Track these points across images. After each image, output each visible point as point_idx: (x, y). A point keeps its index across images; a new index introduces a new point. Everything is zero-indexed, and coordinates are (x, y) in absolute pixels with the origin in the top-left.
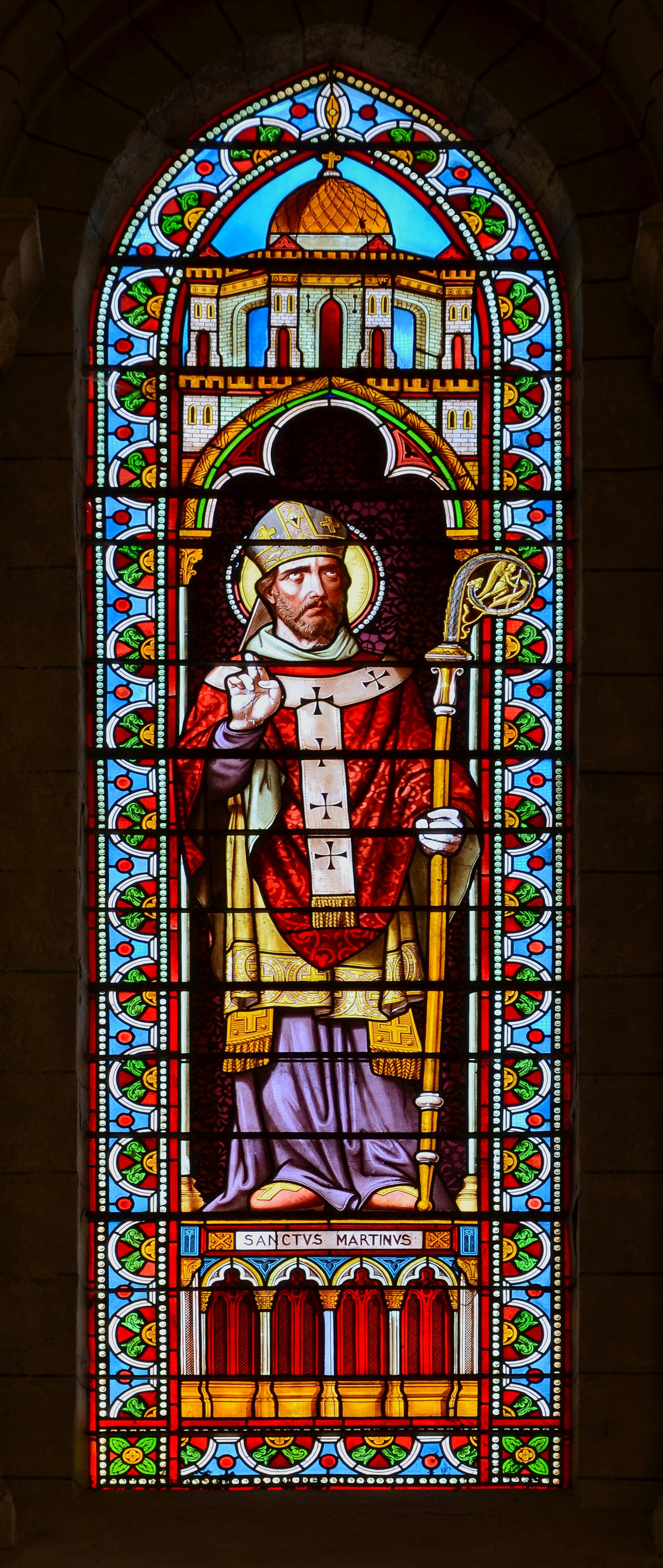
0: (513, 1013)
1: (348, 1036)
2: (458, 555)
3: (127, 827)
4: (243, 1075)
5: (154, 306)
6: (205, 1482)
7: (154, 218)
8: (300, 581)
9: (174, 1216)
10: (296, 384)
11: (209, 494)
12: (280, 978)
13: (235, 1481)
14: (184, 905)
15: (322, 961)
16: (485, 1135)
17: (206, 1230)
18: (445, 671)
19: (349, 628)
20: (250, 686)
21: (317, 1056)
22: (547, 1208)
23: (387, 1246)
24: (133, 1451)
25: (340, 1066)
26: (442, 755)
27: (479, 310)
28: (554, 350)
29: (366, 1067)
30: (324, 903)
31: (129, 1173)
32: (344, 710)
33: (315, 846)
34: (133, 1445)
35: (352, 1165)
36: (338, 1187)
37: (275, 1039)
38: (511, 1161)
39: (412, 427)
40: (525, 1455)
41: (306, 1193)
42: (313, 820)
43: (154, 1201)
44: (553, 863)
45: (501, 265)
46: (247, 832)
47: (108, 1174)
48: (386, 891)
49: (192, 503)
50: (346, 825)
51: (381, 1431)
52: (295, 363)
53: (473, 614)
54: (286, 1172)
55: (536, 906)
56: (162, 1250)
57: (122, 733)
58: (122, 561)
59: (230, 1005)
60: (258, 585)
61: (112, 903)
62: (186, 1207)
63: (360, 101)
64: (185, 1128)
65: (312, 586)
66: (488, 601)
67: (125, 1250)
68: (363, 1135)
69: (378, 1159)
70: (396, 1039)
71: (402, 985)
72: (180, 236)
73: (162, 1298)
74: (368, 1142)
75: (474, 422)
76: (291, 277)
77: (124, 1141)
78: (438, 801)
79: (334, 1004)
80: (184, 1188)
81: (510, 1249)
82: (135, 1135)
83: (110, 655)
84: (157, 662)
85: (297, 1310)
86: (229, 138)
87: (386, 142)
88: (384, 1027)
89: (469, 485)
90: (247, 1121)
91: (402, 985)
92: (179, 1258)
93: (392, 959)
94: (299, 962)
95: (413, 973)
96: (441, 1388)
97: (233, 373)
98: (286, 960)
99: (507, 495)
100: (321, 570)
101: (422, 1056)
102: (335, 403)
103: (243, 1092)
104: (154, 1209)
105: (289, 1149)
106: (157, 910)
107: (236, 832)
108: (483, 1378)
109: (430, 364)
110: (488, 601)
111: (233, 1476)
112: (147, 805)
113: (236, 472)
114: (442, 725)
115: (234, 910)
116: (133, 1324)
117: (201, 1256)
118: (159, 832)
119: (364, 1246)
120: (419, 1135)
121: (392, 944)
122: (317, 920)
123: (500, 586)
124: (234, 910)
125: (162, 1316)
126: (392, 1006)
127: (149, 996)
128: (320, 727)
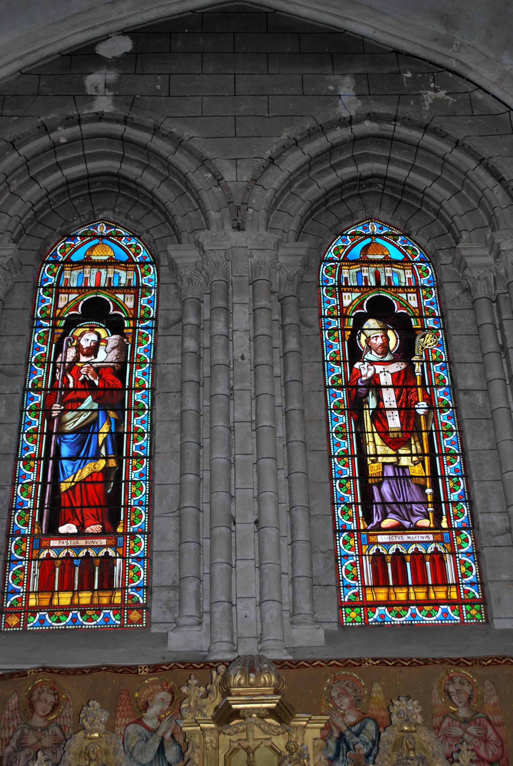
0: (449, 463)
1: (403, 471)
2: (417, 332)
3: (336, 408)
4: (375, 484)
5: (333, 271)
6: (377, 623)
7: (332, 251)
8: (376, 339)
9: (358, 530)
10: (370, 290)
11: (351, 317)
12: (383, 453)
13: (386, 623)
14: (354, 431)
15: (394, 447)
16: (127, 481)
17: (368, 535)
18: (417, 363)
19: (391, 352)
20: (366, 368)
21: (395, 477)
22: (468, 526)
23: (423, 540)
24: (353, 613)
25: (402, 481)
26: (419, 386)
27: (414, 272)
28: (434, 282)
29: (410, 480)
30: (392, 430)
31: (344, 516)
32: (392, 374)
33: (388, 413)
34: (353, 611)
35: (409, 513)
36: (406, 520)
37: (383, 472)
38: (455, 511)
39: (400, 300)
40: (473, 612)
41: (396, 522)
42: (387, 405)
43: (27, 530)
44: (454, 417)
45: (418, 262)
46: (369, 409)
47: (338, 517)
48: (409, 426)
49: (347, 319)
50: (396, 407)
51: (429, 605)
52: (369, 285)
53: (423, 348)
54: (391, 515)
55: (451, 430)
56: (356, 542)
57: (333, 381)
58: (330, 335)
59: (369, 462)
60: (366, 341)
61: (333, 431)
62: (362, 527)
63: (379, 226)
64: (359, 501)
65: (380, 341)
66: (426, 344)
67: (345, 542)
68: (411, 503)
69: (417, 510)
70: (417, 472)
71: (417, 455)
72: (339, 255)
73: (358, 559)
74: (413, 505)
75: (133, 300)
76: (366, 265)
77: (342, 506)
78: (420, 400)
79: (399, 461)
80: (361, 521)
81: (459, 540)
82: (345, 504)
83: (328, 359)
84: (341, 361)
85: (399, 562)
86: (349, 233)
87: (386, 234)
88: (413, 468)
89: (131, 316)
90: (377, 499)
91: (417, 455)
92: (362, 545)
93: (413, 447)
94: (387, 448)
95: (420, 451)
96: (444, 589)
97: (355, 287)
98: (384, 447)
99: (427, 317)
100: (382, 337)
101: (425, 477)
102: (98, 296)
103: (375, 489)
104: (26, 533)
105: (390, 507)
106: (346, 432)
107: (366, 409)
108: (457, 585)
109: (403, 285)
110: (426, 344)
111: (385, 621)
112: (341, 402)
113: (357, 311)
114: (418, 378)
115: (368, 432)
116: (350, 568)
117: (368, 544)
118: (345, 409)
119: (416, 540)
120: (428, 503)
121: (413, 442)
122: (391, 435)
123: (428, 341)
124: (368, 432)
125: (358, 565)
126: (415, 461)
127: (345, 459)
128: (386, 379)
